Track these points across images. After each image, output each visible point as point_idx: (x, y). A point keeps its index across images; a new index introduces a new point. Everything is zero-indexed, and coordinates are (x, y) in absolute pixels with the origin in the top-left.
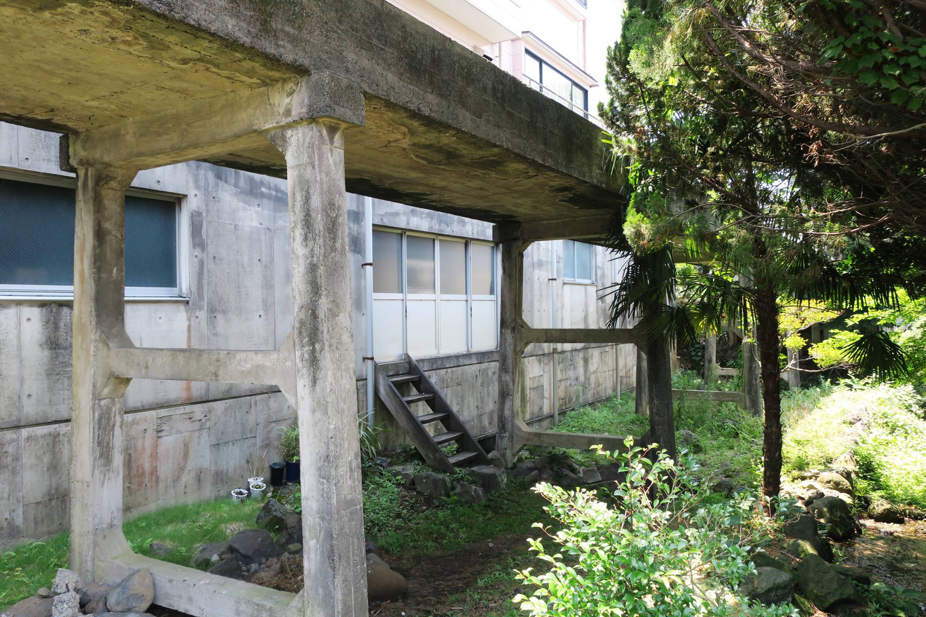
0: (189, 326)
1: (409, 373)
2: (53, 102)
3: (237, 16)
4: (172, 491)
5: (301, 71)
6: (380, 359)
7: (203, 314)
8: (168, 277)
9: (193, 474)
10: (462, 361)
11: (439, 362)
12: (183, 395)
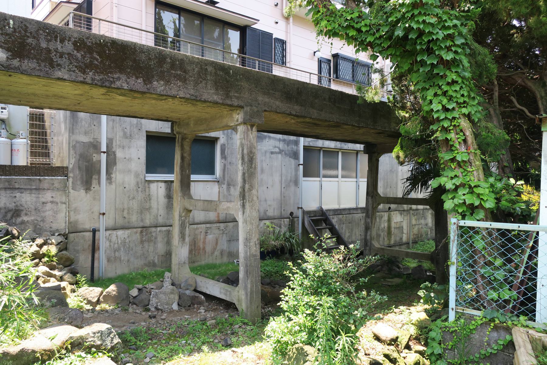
0: (219, 191)
1: (322, 216)
2: (168, 116)
3: (217, 94)
4: (211, 258)
5: (242, 107)
6: (307, 208)
7: (225, 186)
8: (211, 171)
9: (219, 251)
10: (352, 212)
11: (339, 212)
12: (216, 219)
